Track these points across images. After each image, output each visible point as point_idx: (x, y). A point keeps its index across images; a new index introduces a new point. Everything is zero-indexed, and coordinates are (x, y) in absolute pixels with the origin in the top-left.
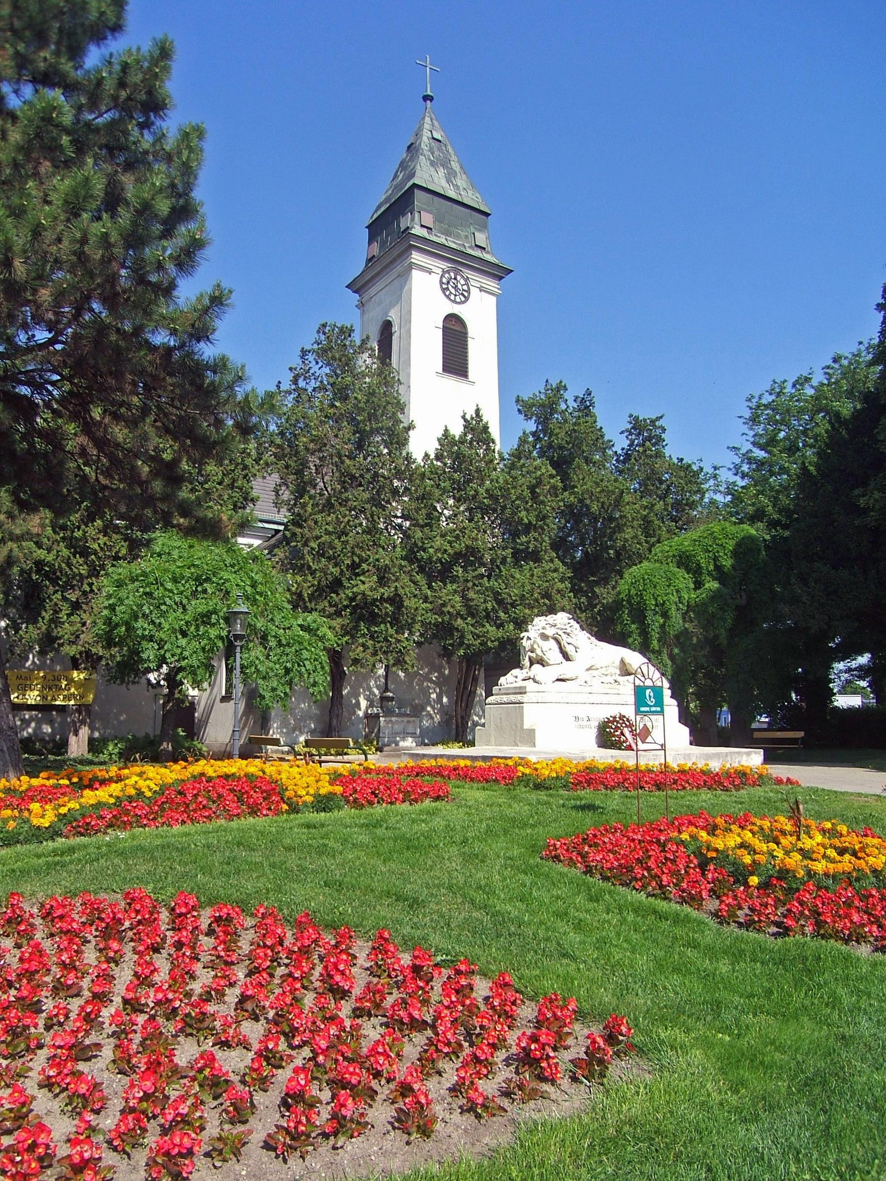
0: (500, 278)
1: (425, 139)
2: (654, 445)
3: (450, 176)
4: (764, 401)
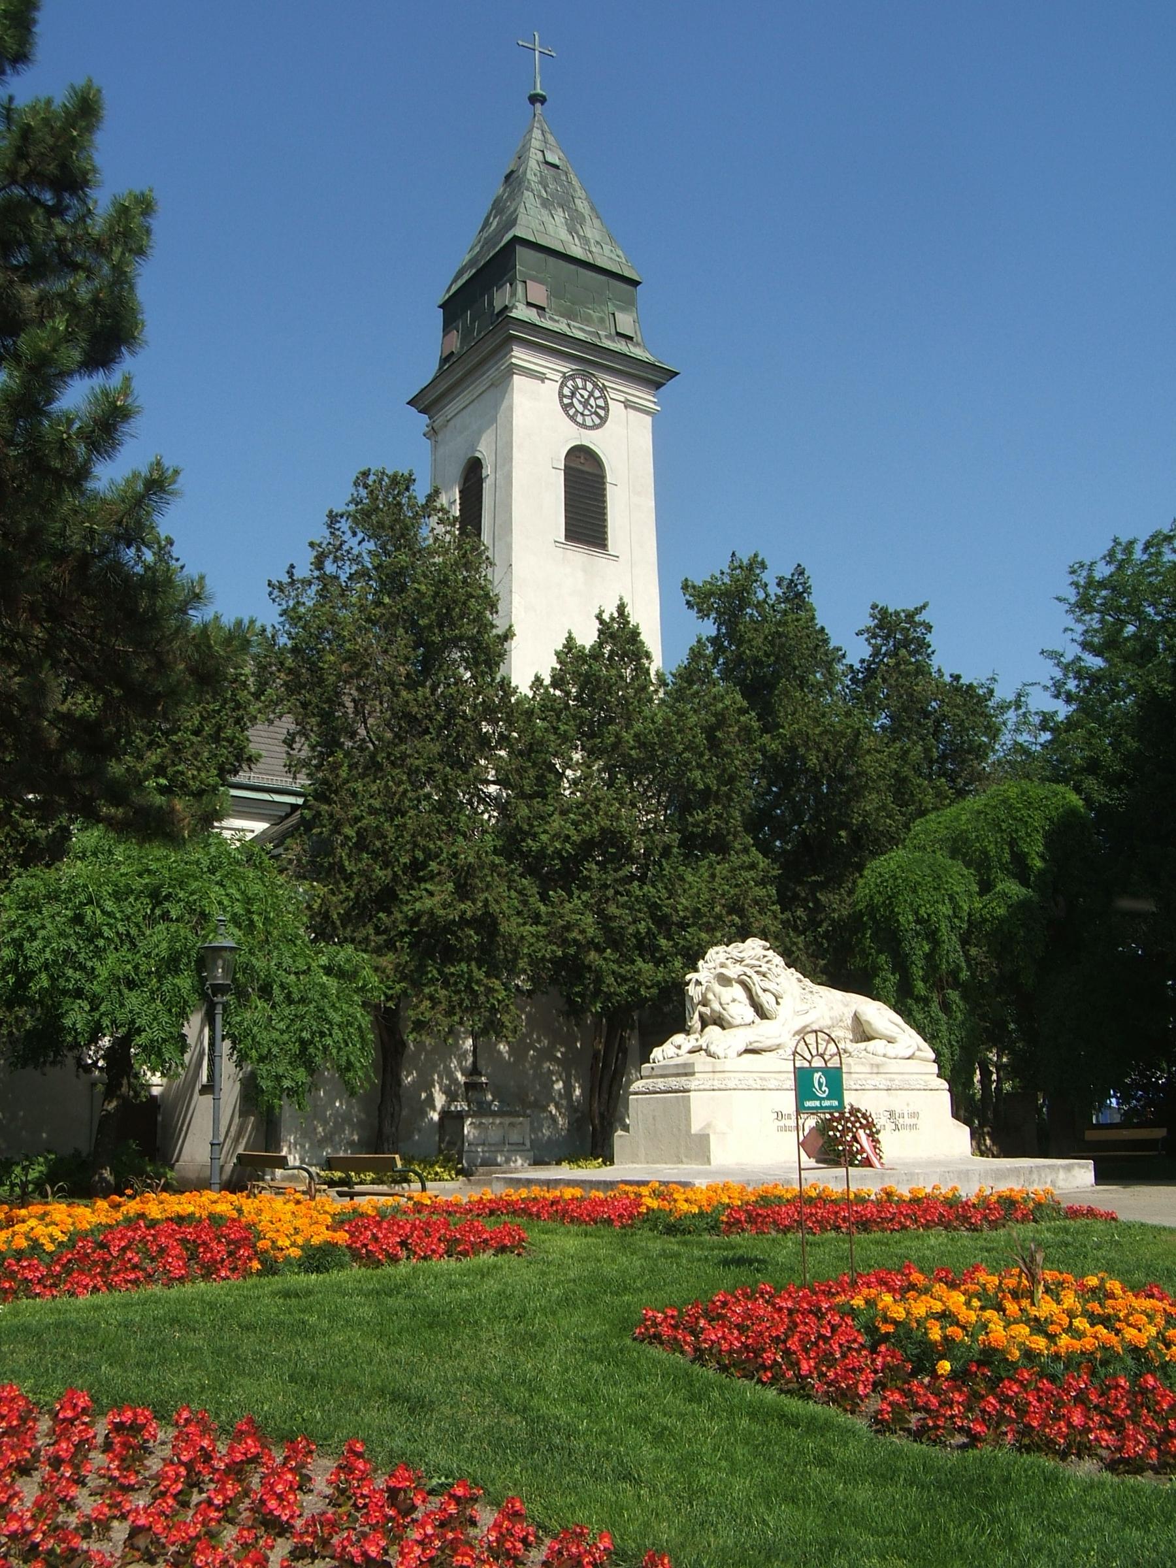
0: (658, 386)
1: (533, 164)
2: (913, 653)
3: (574, 223)
4: (1098, 576)
